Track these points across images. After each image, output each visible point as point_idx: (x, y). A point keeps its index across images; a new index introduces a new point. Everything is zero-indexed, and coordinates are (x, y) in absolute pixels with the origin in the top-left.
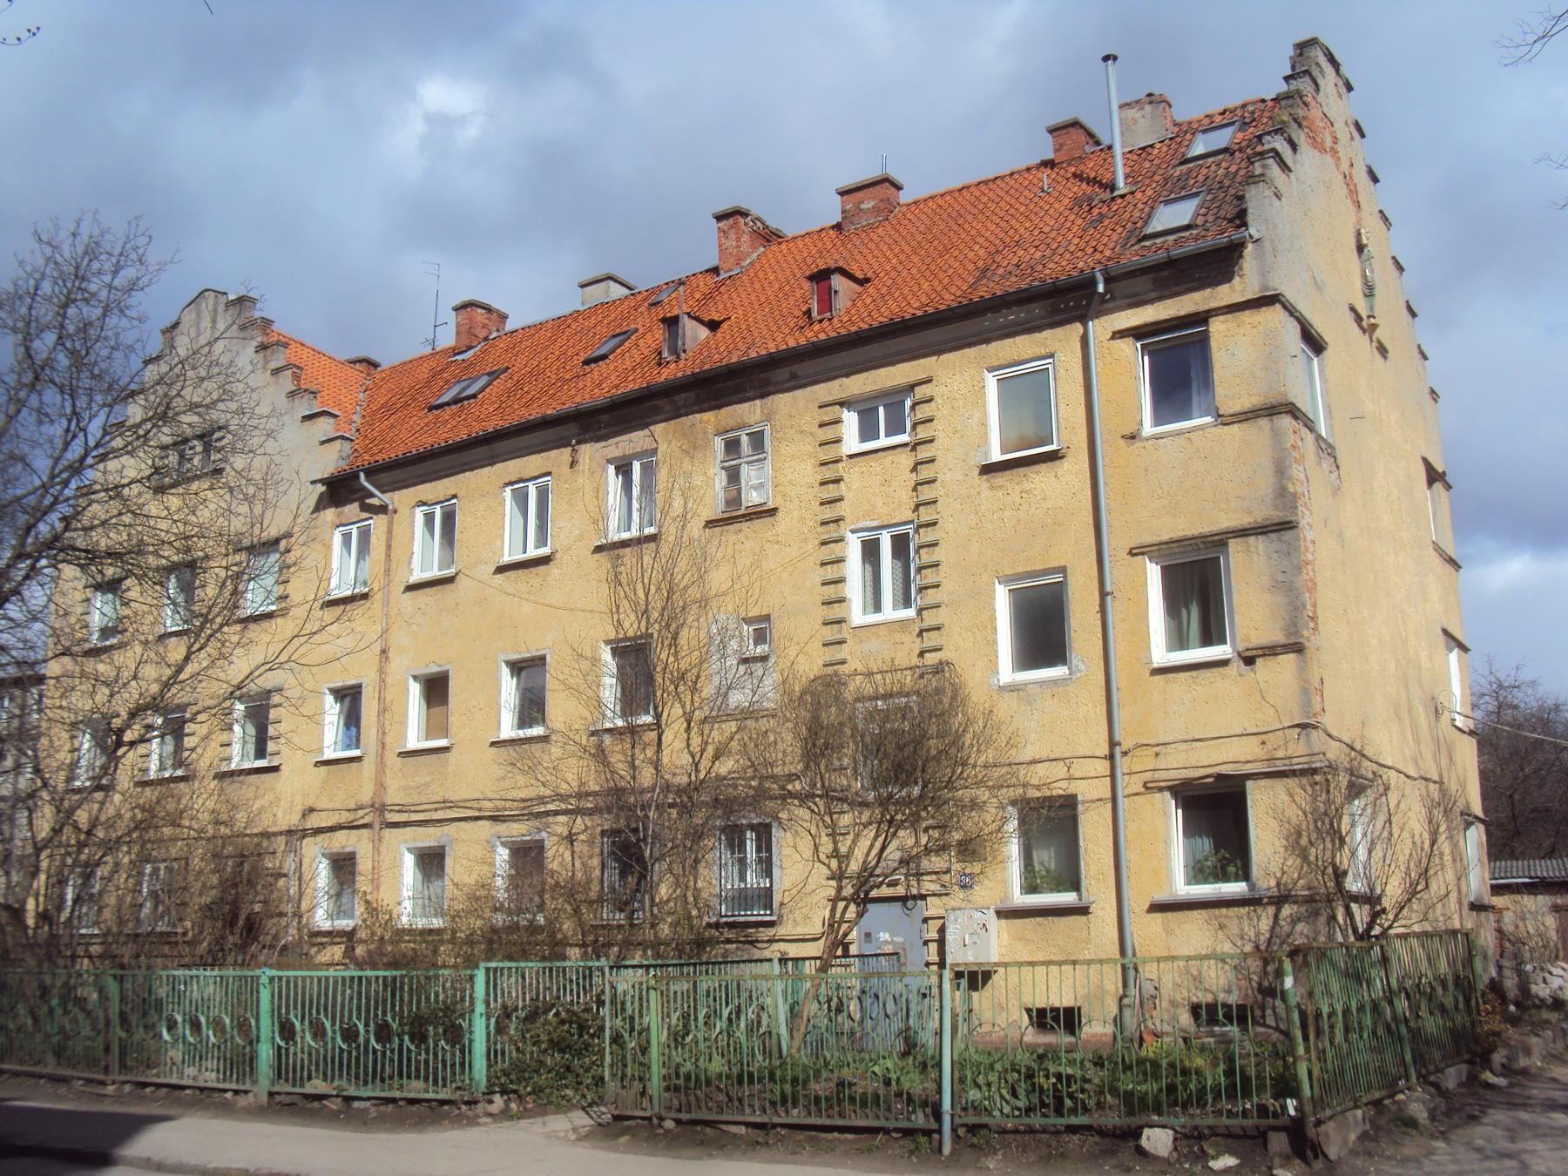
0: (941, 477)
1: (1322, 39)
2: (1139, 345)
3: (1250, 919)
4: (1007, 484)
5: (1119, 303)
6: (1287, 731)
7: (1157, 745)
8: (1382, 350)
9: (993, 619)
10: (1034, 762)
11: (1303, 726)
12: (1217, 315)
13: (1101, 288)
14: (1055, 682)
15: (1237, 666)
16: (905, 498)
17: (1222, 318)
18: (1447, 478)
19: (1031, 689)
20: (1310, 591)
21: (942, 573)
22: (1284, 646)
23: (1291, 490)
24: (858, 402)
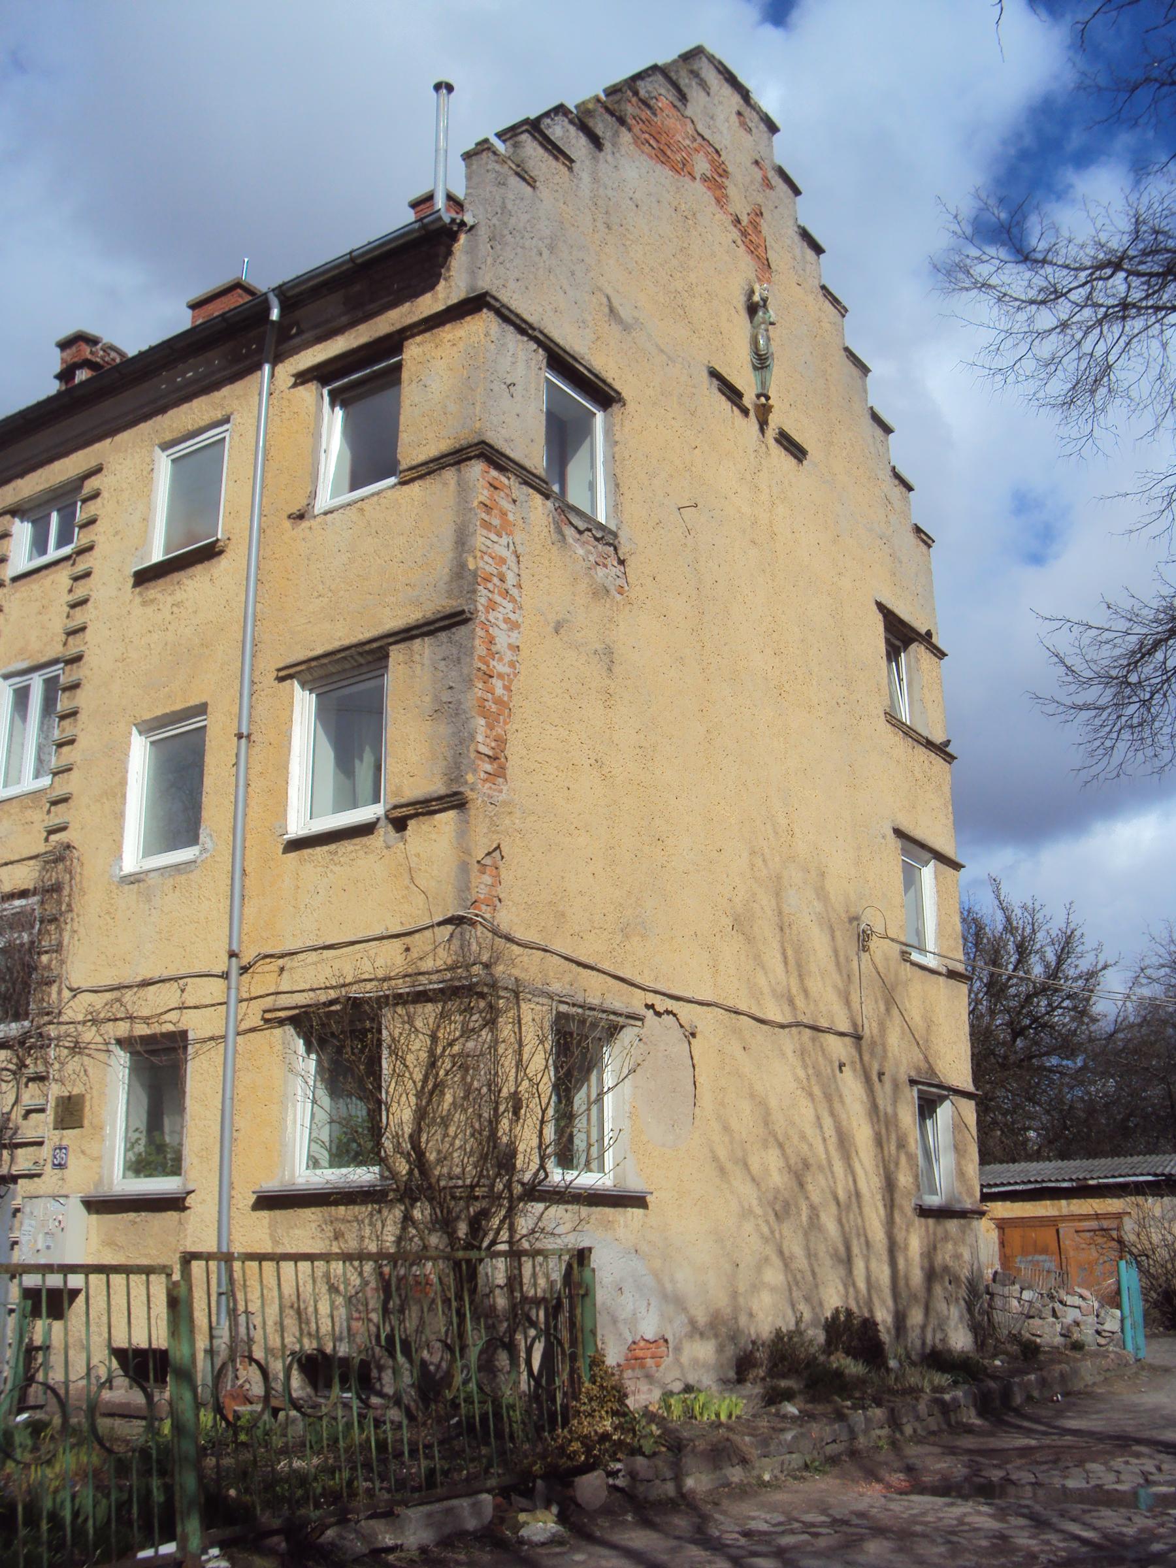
0: (94, 595)
1: (711, 49)
2: (325, 392)
3: (371, 1224)
4: (159, 596)
5: (307, 336)
6: (436, 929)
7: (282, 956)
8: (795, 450)
9: (123, 783)
10: (146, 984)
11: (456, 921)
12: (413, 336)
13: (275, 315)
14: (177, 868)
15: (385, 832)
16: (58, 623)
17: (418, 339)
18: (934, 640)
19: (154, 879)
20: (492, 720)
21: (80, 724)
22: (440, 798)
23: (472, 566)
24: (31, 509)
